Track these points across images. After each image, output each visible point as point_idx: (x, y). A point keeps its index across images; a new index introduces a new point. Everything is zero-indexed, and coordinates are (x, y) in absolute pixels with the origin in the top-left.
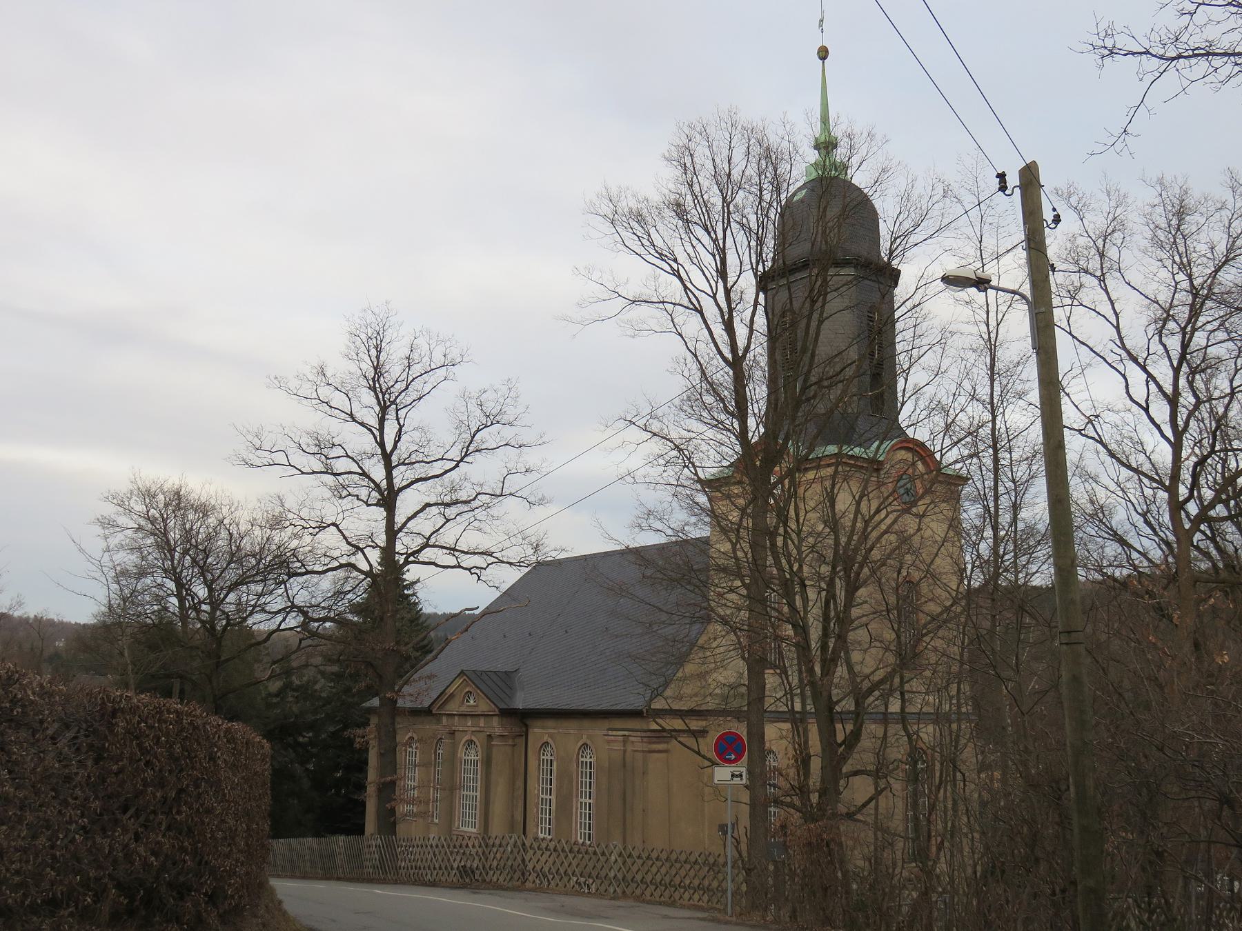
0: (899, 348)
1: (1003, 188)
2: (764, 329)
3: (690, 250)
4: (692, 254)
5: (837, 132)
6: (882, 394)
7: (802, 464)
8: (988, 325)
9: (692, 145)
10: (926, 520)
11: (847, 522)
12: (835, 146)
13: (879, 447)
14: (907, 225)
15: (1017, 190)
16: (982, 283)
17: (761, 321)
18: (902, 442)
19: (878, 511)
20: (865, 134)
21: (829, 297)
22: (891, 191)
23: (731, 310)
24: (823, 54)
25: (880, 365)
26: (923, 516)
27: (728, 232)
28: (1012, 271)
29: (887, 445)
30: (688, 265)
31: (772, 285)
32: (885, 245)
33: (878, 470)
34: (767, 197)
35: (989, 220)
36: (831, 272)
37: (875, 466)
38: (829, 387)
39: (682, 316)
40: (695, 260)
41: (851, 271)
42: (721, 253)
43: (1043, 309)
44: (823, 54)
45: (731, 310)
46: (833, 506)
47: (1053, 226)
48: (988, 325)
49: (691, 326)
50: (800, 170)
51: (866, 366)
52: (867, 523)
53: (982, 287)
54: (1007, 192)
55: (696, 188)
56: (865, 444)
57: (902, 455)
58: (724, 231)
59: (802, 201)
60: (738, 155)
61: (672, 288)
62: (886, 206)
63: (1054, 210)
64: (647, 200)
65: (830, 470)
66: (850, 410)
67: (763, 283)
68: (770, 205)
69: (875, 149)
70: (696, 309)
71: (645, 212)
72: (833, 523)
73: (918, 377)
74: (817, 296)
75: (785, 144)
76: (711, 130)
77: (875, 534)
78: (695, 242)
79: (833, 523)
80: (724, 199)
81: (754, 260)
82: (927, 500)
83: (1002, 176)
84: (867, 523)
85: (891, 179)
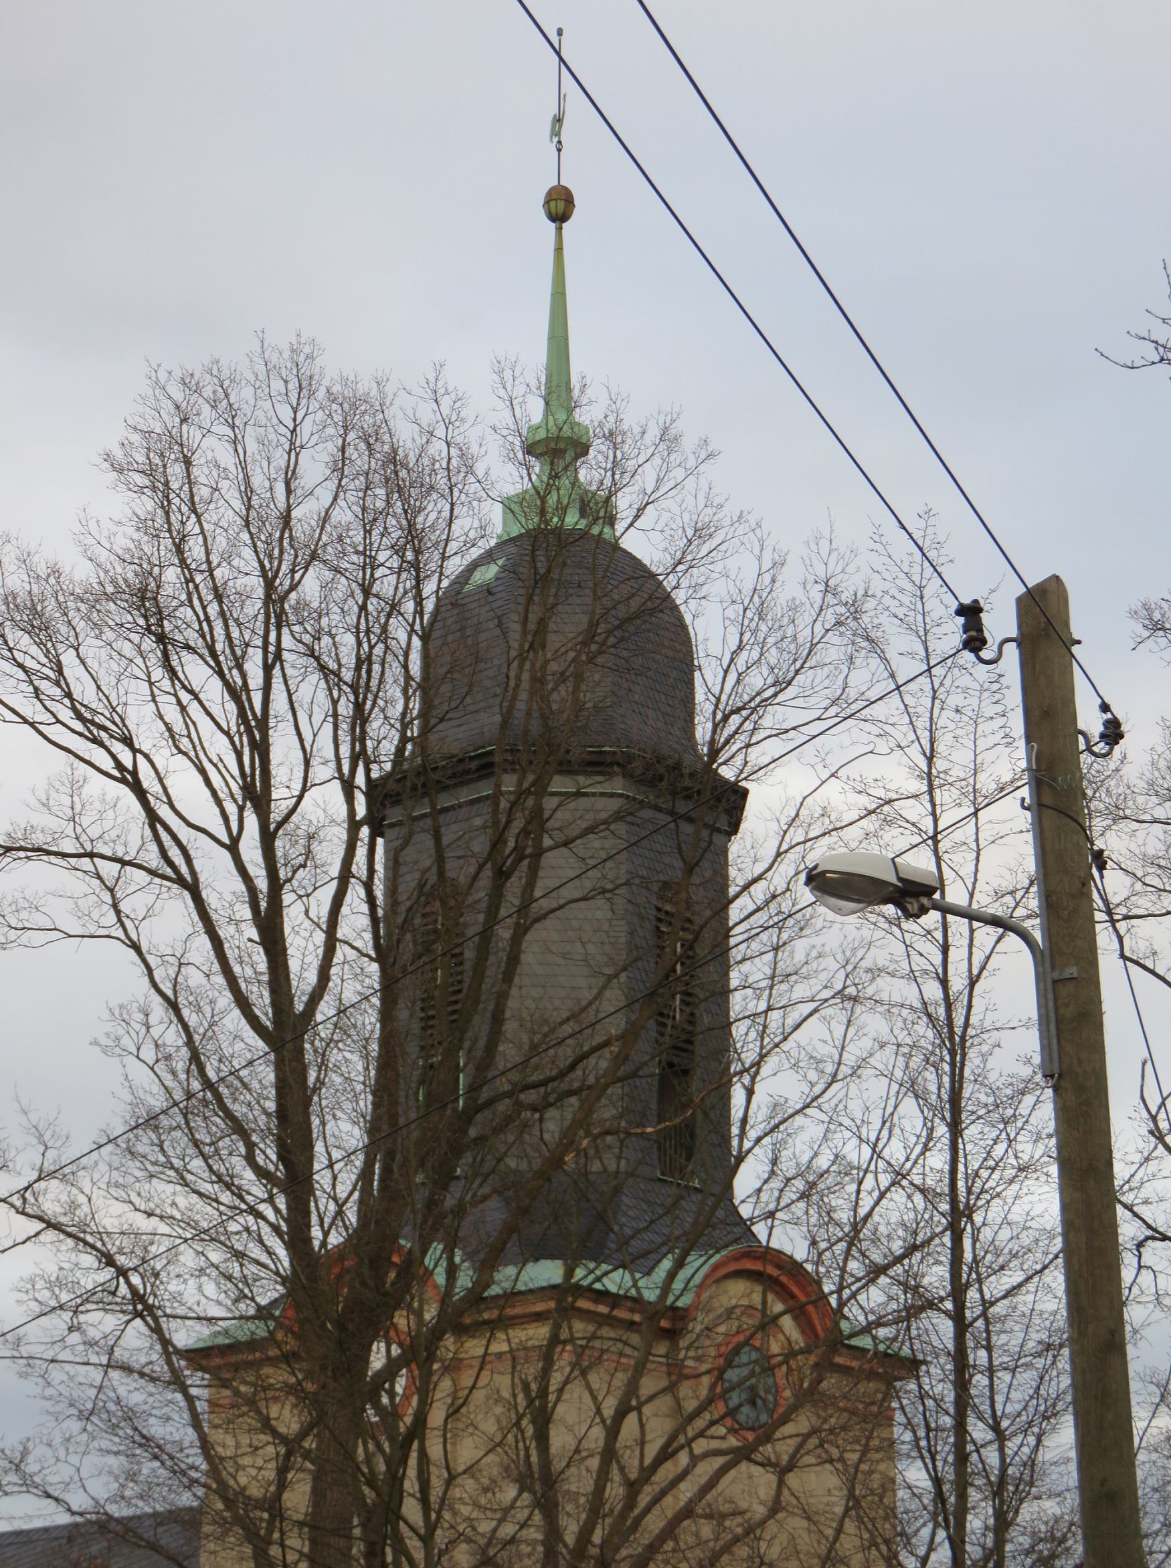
0: (739, 1003)
1: (974, 642)
2: (366, 941)
3: (172, 714)
4: (179, 727)
5: (588, 416)
6: (689, 1128)
7: (471, 1314)
8: (944, 982)
9: (192, 434)
10: (792, 1479)
11: (579, 1482)
12: (582, 449)
13: (672, 1275)
14: (756, 680)
15: (1011, 650)
16: (911, 896)
17: (355, 922)
18: (737, 1258)
19: (666, 1454)
20: (653, 433)
21: (549, 859)
22: (718, 589)
23: (276, 886)
24: (560, 207)
25: (684, 1045)
26: (790, 1467)
27: (277, 672)
28: (1000, 857)
29: (697, 1266)
30: (164, 757)
31: (394, 814)
32: (703, 731)
33: (672, 1335)
34: (386, 585)
35: (954, 700)
36: (560, 784)
37: (667, 1323)
38: (540, 1108)
39: (140, 893)
40: (185, 744)
41: (618, 785)
42: (255, 735)
43: (1073, 971)
44: (560, 207)
45: (276, 886)
46: (542, 1437)
47: (1101, 748)
48: (944, 982)
49: (168, 921)
50: (477, 524)
51: (643, 1050)
52: (633, 1488)
53: (913, 907)
54: (985, 654)
55: (195, 550)
56: (638, 1261)
57: (738, 1292)
58: (268, 669)
59: (488, 590)
60: (314, 468)
61: (117, 817)
62: (710, 629)
63: (1105, 708)
64: (56, 572)
65: (539, 1333)
66: (596, 1166)
67: (388, 803)
68: (394, 608)
69: (679, 474)
70: (180, 880)
71: (50, 606)
72: (542, 1485)
73: (779, 1084)
74: (514, 855)
75: (437, 448)
76: (243, 396)
77: (654, 1523)
78: (185, 697)
79: (542, 1485)
80: (269, 585)
81: (345, 751)
82: (802, 1423)
83: (971, 613)
84: (633, 1488)
85: (745, 523)
